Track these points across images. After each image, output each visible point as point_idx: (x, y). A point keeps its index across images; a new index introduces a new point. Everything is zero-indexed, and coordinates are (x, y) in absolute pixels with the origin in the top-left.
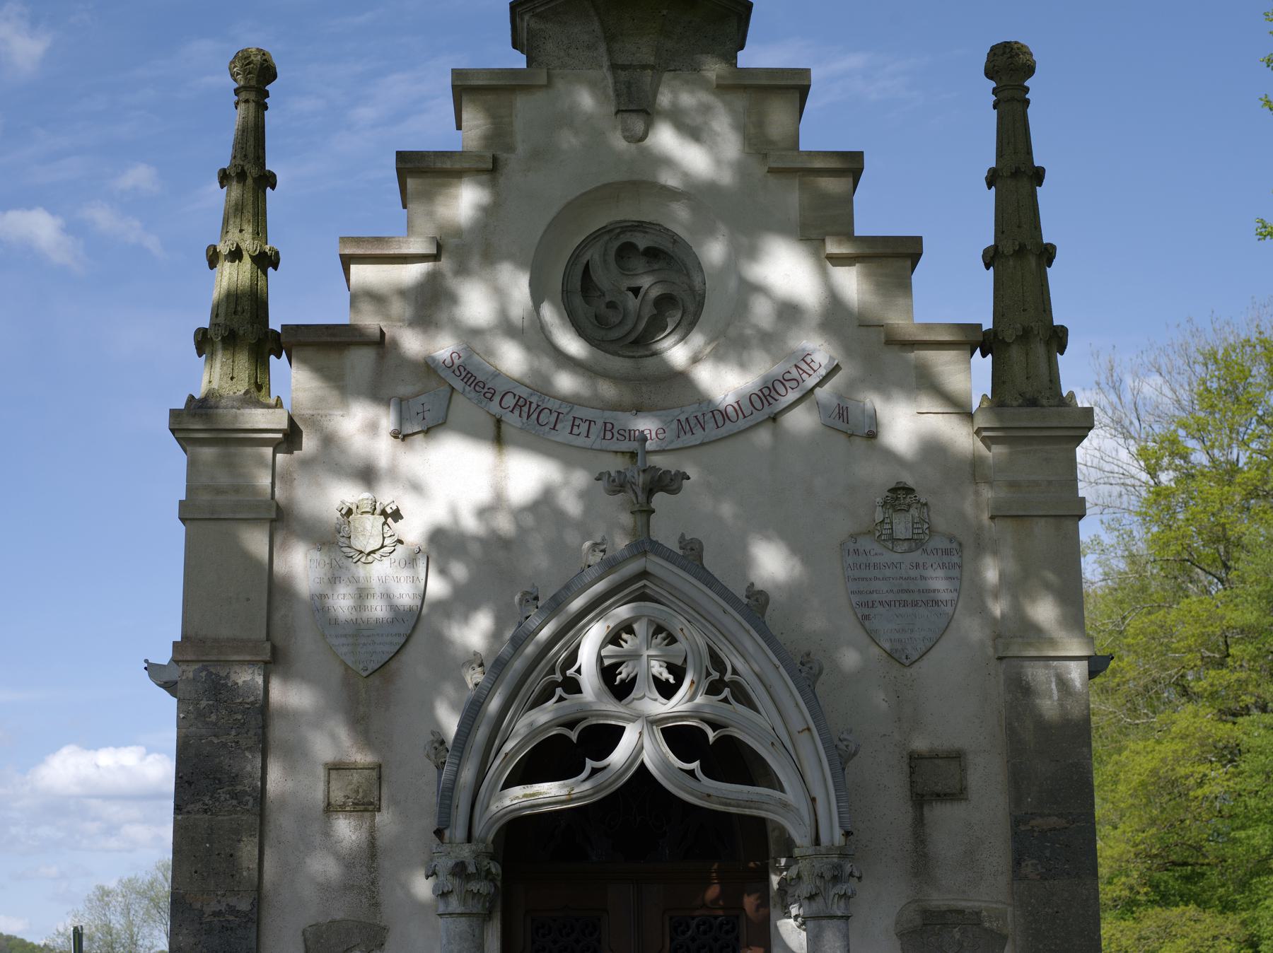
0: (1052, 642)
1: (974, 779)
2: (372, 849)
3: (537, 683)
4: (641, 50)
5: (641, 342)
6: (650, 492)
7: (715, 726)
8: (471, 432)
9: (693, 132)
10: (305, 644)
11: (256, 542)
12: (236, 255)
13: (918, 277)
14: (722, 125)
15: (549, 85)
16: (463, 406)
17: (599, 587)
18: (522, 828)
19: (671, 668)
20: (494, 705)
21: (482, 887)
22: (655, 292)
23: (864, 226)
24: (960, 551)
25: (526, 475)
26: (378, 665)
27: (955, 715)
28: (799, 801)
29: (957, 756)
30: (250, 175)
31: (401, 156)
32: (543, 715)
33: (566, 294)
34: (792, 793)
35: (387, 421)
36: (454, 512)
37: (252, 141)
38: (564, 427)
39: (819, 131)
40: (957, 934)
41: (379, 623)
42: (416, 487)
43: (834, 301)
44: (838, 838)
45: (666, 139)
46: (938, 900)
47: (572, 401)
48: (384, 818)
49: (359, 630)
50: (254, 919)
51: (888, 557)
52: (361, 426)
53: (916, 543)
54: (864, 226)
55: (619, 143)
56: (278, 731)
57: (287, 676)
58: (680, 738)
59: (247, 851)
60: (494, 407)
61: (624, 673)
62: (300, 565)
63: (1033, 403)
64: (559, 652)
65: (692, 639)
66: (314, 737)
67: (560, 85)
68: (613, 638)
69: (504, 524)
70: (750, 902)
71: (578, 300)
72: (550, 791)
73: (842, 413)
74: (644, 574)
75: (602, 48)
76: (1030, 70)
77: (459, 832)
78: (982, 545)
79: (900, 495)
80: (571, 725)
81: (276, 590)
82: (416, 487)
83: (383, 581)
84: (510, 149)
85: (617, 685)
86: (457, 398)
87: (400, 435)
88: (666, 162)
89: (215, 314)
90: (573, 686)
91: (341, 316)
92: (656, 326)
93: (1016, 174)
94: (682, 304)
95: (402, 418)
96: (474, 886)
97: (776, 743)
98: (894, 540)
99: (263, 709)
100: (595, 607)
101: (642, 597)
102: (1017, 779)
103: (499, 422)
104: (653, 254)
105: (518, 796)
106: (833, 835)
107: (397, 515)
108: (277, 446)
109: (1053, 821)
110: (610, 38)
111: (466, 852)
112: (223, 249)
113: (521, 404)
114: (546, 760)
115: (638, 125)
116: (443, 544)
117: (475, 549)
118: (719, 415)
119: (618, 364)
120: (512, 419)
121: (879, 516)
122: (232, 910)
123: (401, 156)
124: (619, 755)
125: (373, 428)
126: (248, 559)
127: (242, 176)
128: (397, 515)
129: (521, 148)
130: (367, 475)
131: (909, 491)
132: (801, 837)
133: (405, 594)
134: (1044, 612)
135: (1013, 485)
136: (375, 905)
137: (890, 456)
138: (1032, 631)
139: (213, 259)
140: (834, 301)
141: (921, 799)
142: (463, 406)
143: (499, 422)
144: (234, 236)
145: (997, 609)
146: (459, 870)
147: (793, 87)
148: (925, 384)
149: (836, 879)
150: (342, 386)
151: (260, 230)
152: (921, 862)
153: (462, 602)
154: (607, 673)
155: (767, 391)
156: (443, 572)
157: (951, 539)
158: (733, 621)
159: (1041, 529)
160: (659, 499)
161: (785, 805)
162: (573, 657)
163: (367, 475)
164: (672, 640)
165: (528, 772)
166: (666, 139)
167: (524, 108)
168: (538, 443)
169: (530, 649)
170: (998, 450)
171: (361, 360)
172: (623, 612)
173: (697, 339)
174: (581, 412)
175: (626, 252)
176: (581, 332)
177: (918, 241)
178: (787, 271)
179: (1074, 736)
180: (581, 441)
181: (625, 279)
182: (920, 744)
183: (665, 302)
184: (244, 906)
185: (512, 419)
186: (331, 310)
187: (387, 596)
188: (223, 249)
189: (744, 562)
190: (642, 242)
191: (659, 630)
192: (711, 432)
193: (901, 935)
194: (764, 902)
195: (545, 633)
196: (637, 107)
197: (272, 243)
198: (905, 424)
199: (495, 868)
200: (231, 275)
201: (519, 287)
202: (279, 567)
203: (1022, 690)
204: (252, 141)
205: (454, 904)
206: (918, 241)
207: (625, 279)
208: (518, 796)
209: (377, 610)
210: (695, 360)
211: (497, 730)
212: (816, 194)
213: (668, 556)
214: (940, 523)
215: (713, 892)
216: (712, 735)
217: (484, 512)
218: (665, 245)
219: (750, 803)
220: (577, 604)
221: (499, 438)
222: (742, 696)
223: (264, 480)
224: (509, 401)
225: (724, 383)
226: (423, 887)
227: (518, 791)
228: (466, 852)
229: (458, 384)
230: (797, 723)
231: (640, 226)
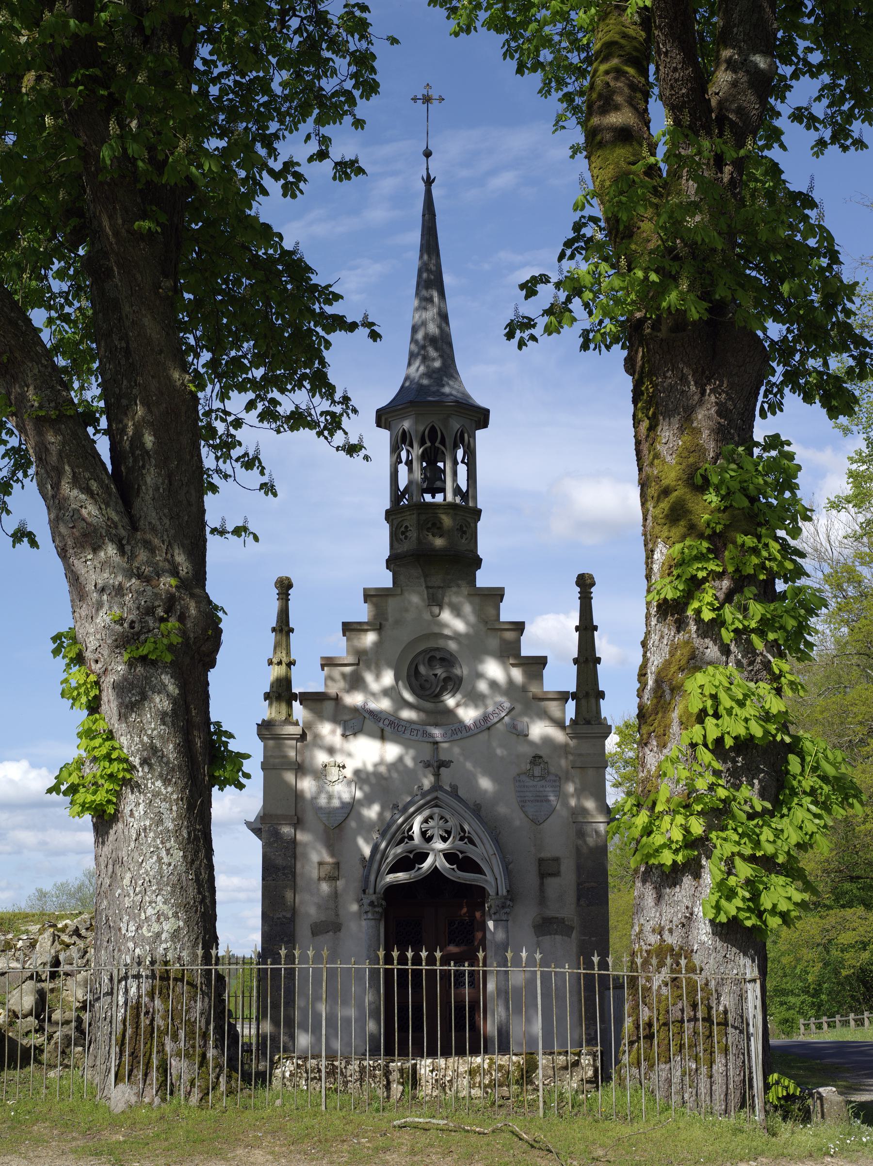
0: (592, 816)
1: (563, 868)
2: (335, 895)
3: (399, 836)
4: (436, 580)
5: (436, 697)
6: (439, 767)
7: (462, 852)
8: (371, 735)
9: (457, 612)
10: (309, 816)
11: (290, 777)
12: (280, 663)
13: (545, 672)
14: (467, 609)
15: (402, 594)
16: (369, 724)
17: (421, 802)
18: (393, 889)
19: (447, 832)
20: (383, 845)
21: (379, 910)
22: (444, 675)
23: (525, 652)
24: (559, 781)
25: (392, 751)
26: (338, 824)
27: (556, 842)
28: (492, 880)
29: (557, 860)
30: (283, 628)
31: (344, 624)
32: (399, 850)
33: (408, 676)
34: (489, 877)
35: (339, 731)
36: (364, 765)
37: (284, 615)
38: (408, 732)
39: (508, 613)
40: (555, 926)
41: (337, 808)
42: (349, 755)
43: (510, 682)
44: (505, 893)
45: (446, 616)
46: (550, 913)
47: (410, 722)
48: (340, 884)
49: (330, 812)
50: (292, 920)
51: (532, 783)
52: (328, 731)
53: (542, 778)
54: (525, 652)
55: (427, 616)
56: (299, 850)
57: (303, 830)
58: (449, 856)
59: (289, 895)
60: (381, 725)
61: (429, 833)
62: (307, 785)
63: (588, 723)
64: (406, 827)
65: (452, 823)
66: (315, 856)
67: (406, 594)
68: (426, 821)
69: (382, 769)
70: (478, 914)
71: (413, 679)
72: (401, 876)
73: (514, 727)
74: (437, 798)
75: (422, 580)
76: (593, 584)
77: (371, 891)
78: (568, 778)
79: (536, 759)
80: (410, 852)
81: (298, 796)
82: (349, 755)
83: (339, 793)
84: (386, 620)
85: (427, 838)
86: (367, 721)
87: (344, 736)
88: (445, 625)
89: (272, 686)
90: (411, 838)
91: (321, 689)
92: (443, 689)
93: (586, 629)
94: (453, 684)
95: (345, 729)
96: (377, 909)
97: (483, 859)
98: (533, 776)
99: (294, 841)
100: (418, 811)
101: (436, 806)
102: (579, 868)
103: (382, 730)
104: (442, 660)
105: (390, 878)
106: (503, 891)
107: (344, 767)
108: (297, 740)
109: (593, 884)
110: (426, 576)
111: (374, 898)
112: (275, 661)
113: (391, 723)
114: (401, 865)
115: (436, 610)
116: (360, 777)
117: (373, 780)
118: (466, 728)
119: (428, 705)
120: (388, 730)
121: (528, 767)
122: (284, 917)
123: (344, 624)
124: (426, 865)
125: (333, 732)
126: (287, 784)
127: (281, 631)
128: (344, 767)
129: (391, 620)
130: (331, 751)
131: (540, 757)
132: (491, 891)
133: (346, 797)
134: (590, 804)
135: (580, 755)
136: (337, 915)
137: (532, 744)
138: (584, 811)
139: (270, 663)
140: (510, 682)
141: (543, 875)
142: (369, 724)
143: (382, 730)
144: (279, 654)
145: (573, 802)
146: (372, 904)
147: (497, 595)
148: (544, 715)
149: (503, 907)
150: (321, 716)
151: (288, 653)
152: (542, 900)
153: (369, 800)
154: (423, 833)
155: (485, 718)
156: (361, 789)
157: (556, 776)
158: (468, 815)
159: (591, 772)
160: (443, 769)
161: (486, 881)
162: (411, 828)
163: (331, 751)
164: (447, 821)
165: (393, 870)
166: (446, 616)
167: (392, 604)
168: (396, 740)
169: (394, 828)
170: (575, 741)
171: (329, 706)
172: (426, 813)
173: (459, 696)
174: (414, 726)
175: (432, 659)
176: (413, 691)
177: (546, 658)
178: (493, 669)
179: (602, 850)
180: (414, 738)
181: (431, 673)
182: (542, 855)
183: (447, 679)
184: (289, 915)
185: (388, 730)
186: (316, 686)
187: (340, 798)
188: (275, 661)
189: (475, 787)
190: (438, 655)
191: (442, 818)
192: (464, 734)
193: (534, 927)
194: (483, 915)
195: (400, 820)
196: (436, 601)
197: (293, 657)
198: (539, 730)
199: (384, 903)
200: (276, 672)
201: (388, 678)
202: (299, 786)
203: (581, 834)
204: (284, 615)
205: (370, 916)
206: (546, 658)
207: (431, 673)
208: (390, 878)
209: (336, 803)
210: (458, 705)
211: (384, 855)
212: (507, 640)
213: (446, 792)
214: (552, 770)
215: (465, 910)
216: (461, 856)
217: (376, 765)
218: (448, 656)
219: (474, 880)
220: (412, 810)
221: (383, 737)
222: (471, 842)
223: (292, 754)
224: (387, 722)
225: (468, 715)
226: (355, 907)
227: (391, 876)
228: (374, 898)
229: (367, 716)
230: (491, 852)
231: (438, 649)
